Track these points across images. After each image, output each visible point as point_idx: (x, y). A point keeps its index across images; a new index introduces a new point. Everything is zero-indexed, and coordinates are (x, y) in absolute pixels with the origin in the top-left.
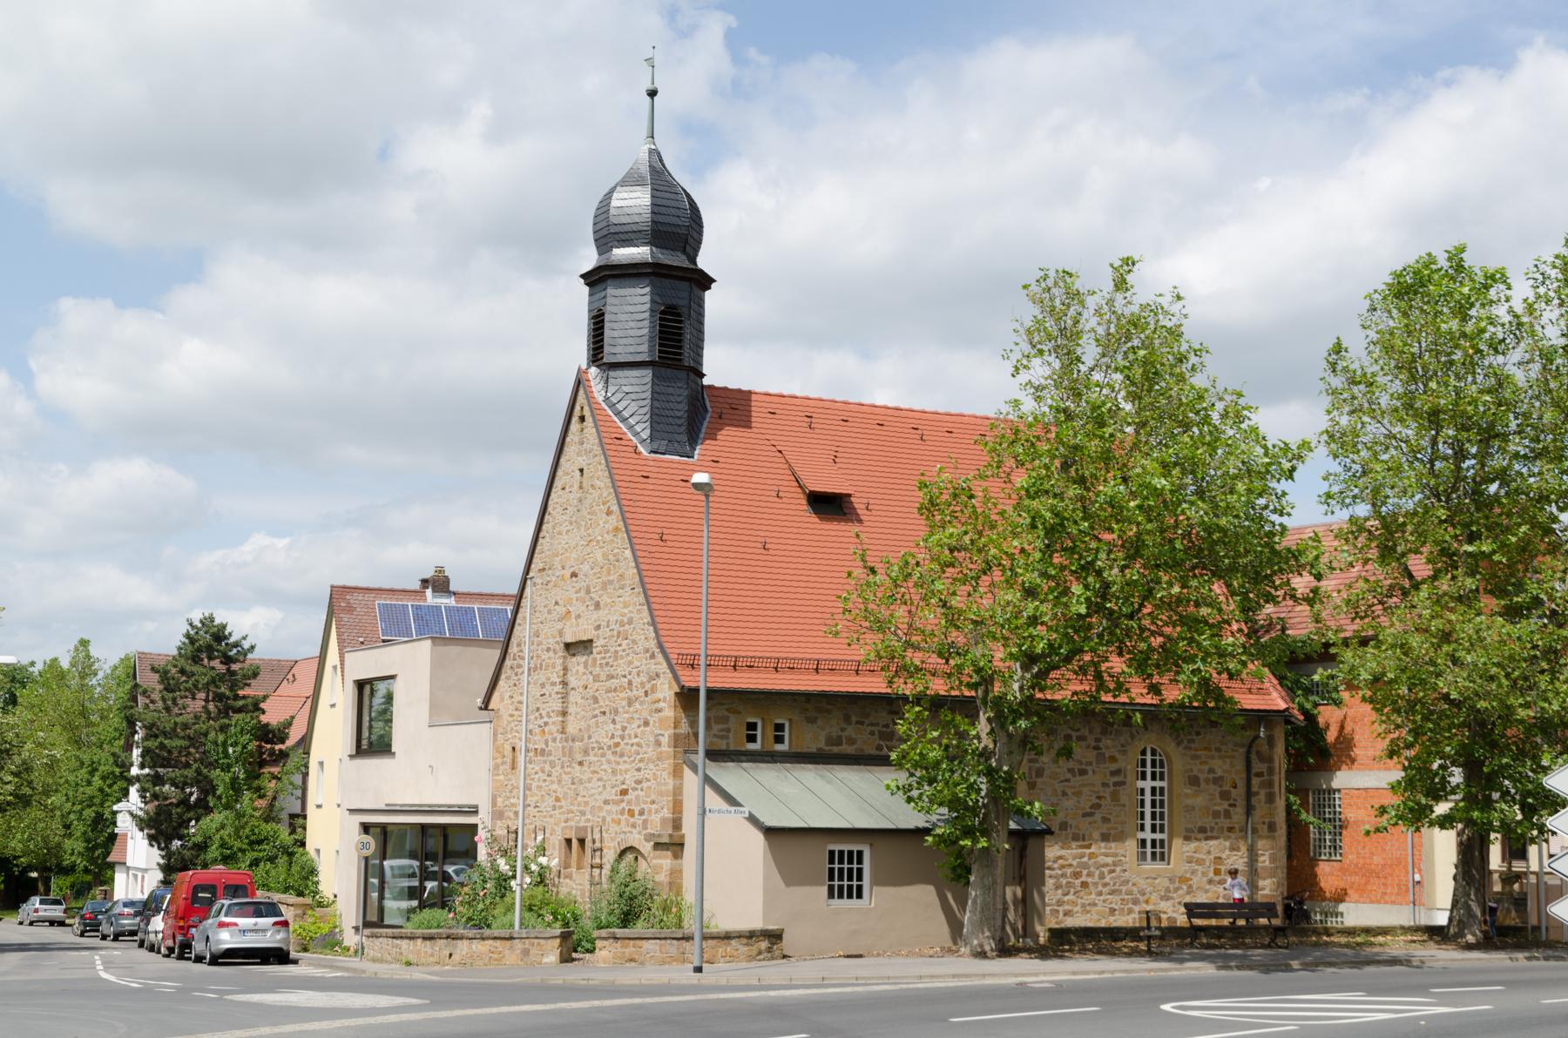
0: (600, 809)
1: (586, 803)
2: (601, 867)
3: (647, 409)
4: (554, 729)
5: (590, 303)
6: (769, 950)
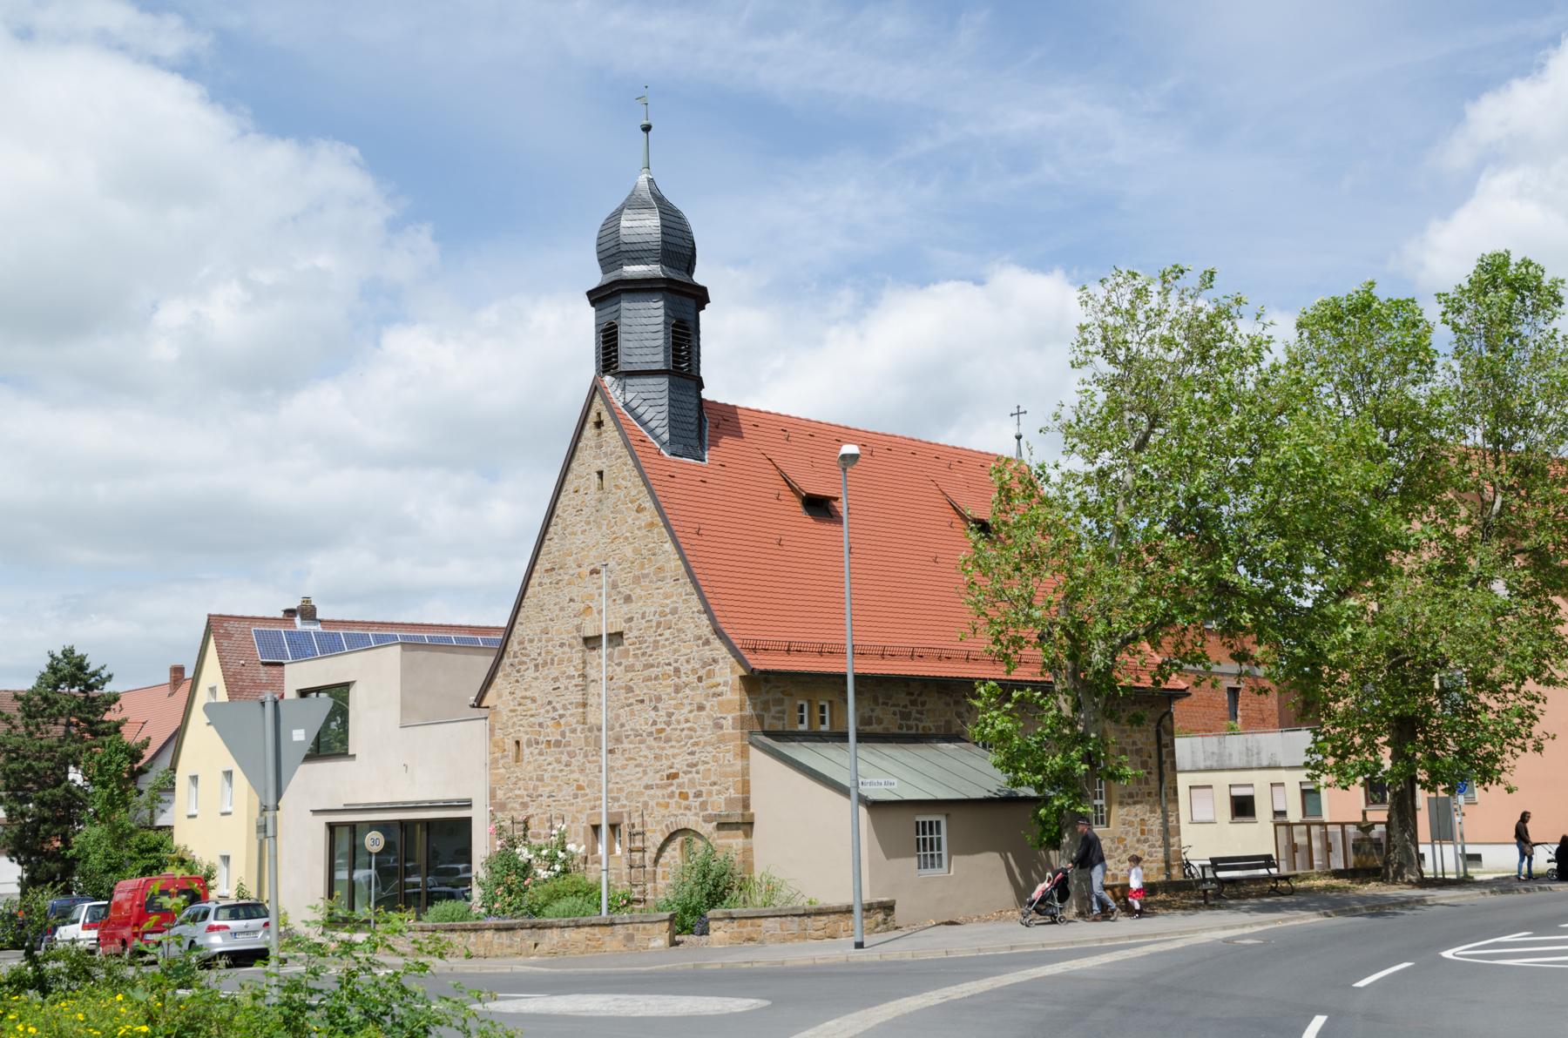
0: (640, 794)
1: (621, 790)
2: (643, 850)
3: (665, 414)
4: (573, 720)
5: (597, 318)
6: (885, 922)
